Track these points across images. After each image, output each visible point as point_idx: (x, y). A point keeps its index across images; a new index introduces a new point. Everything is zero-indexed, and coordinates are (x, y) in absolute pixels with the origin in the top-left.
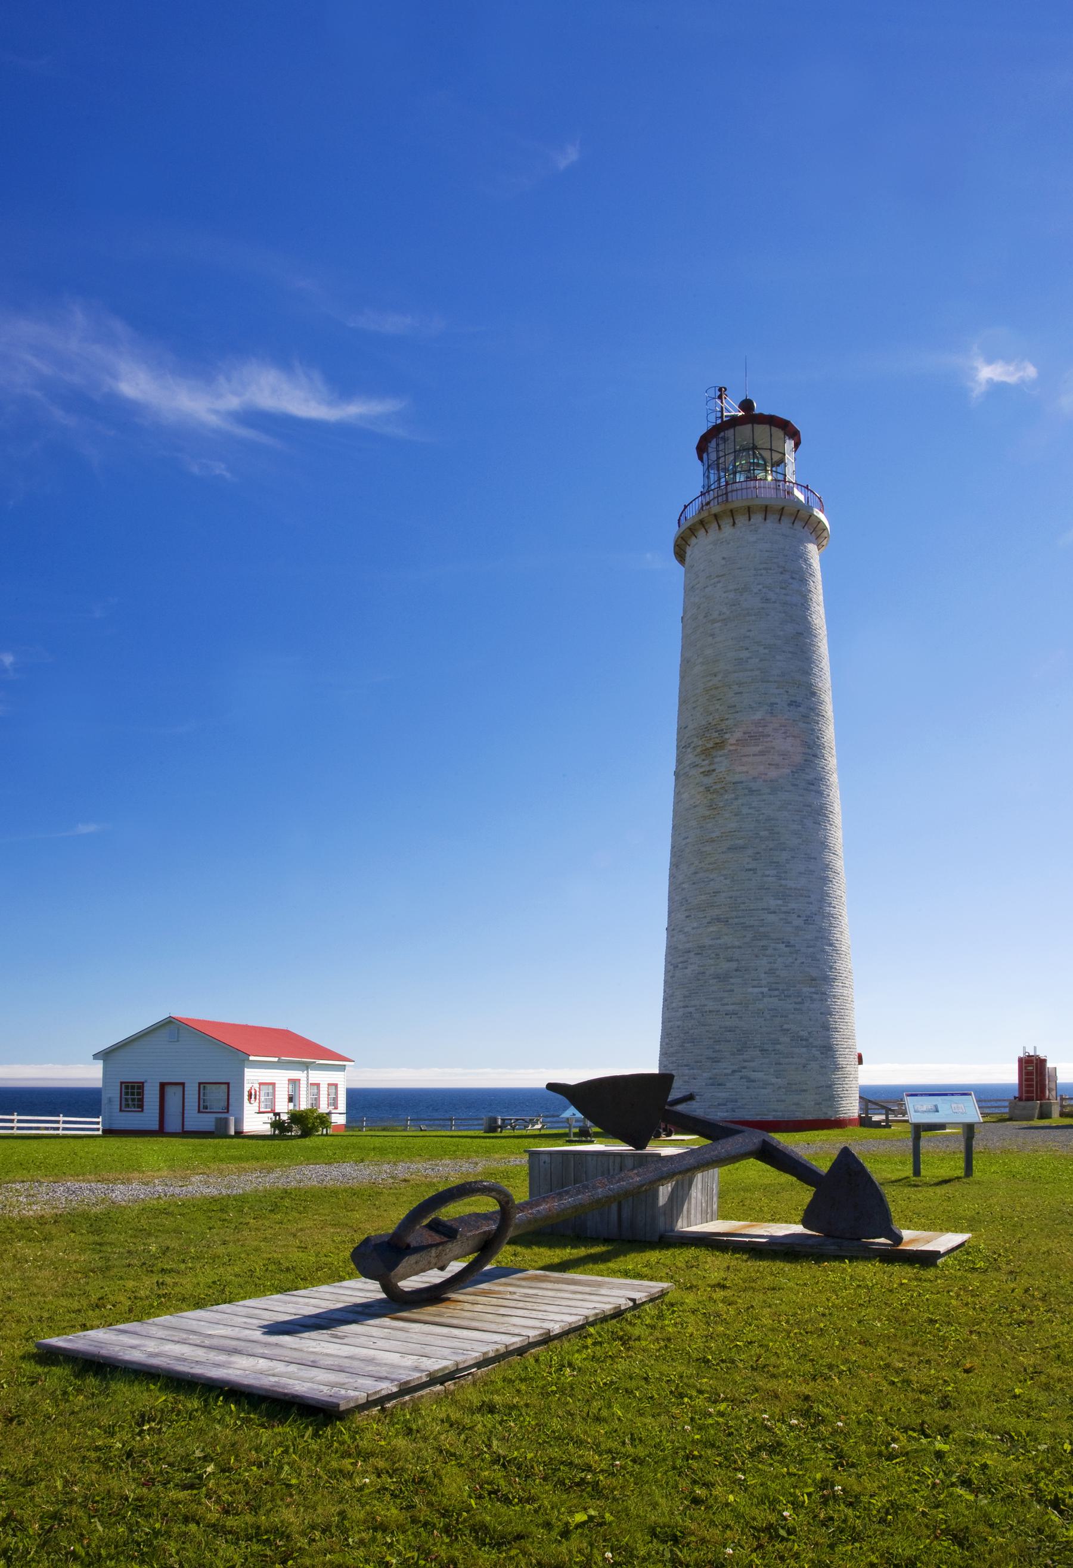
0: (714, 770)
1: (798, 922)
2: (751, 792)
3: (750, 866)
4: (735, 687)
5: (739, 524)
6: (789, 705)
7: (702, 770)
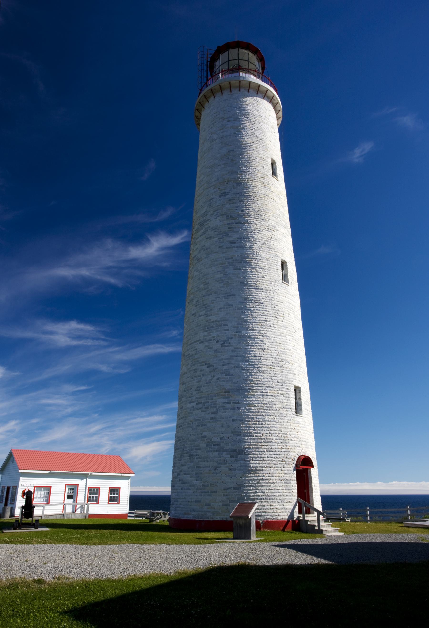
1: (217, 346)
6: (220, 196)
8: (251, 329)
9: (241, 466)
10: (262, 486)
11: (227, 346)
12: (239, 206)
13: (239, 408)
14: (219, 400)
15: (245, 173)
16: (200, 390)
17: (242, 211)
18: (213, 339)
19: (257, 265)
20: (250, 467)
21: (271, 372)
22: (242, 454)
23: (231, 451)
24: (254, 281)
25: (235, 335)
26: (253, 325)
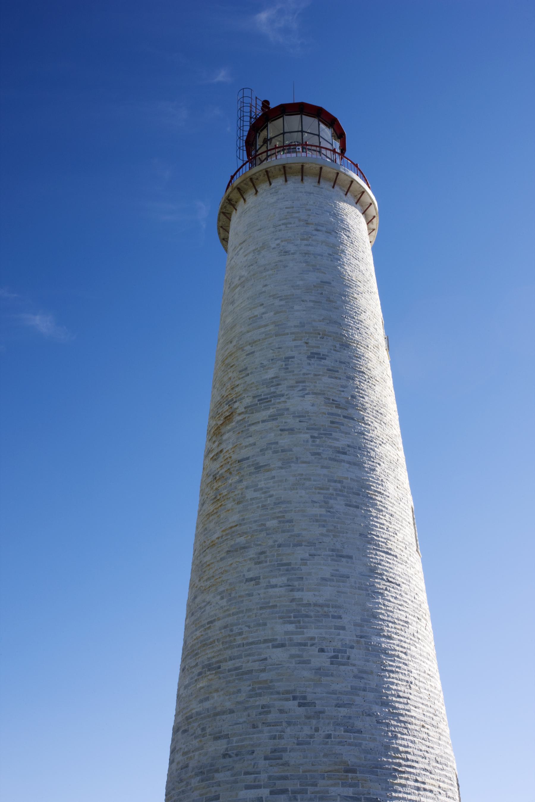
1: (321, 661)
2: (258, 468)
3: (251, 575)
4: (248, 348)
6: (309, 357)
8: (386, 634)
11: (344, 665)
14: (332, 789)
16: (280, 758)
17: (353, 397)
18: (309, 643)
19: (384, 507)
24: (382, 537)
25: (358, 642)
26: (388, 626)
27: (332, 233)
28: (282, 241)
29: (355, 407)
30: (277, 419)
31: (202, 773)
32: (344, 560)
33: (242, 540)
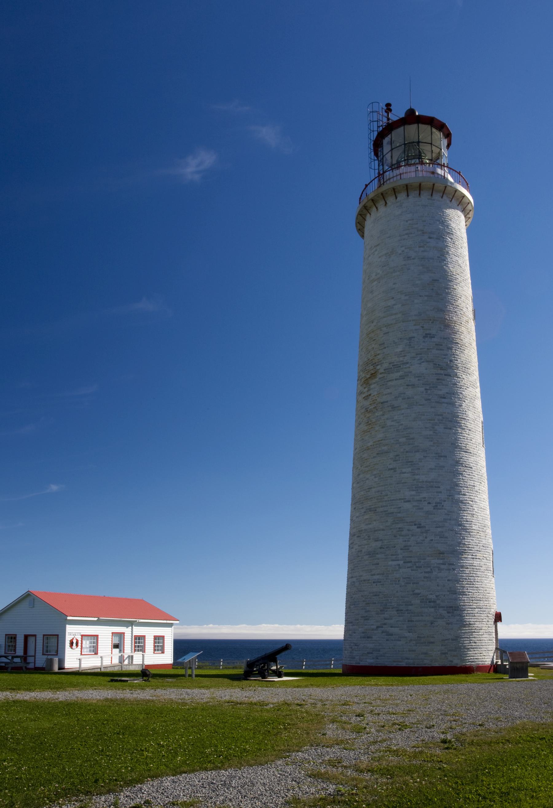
0: (370, 395)
2: (394, 408)
3: (391, 467)
4: (384, 329)
5: (389, 203)
6: (424, 337)
7: (364, 396)
9: (457, 621)
10: (475, 637)
12: (447, 355)
13: (454, 570)
15: (452, 313)
17: (451, 361)
18: (423, 500)
20: (465, 622)
21: (479, 537)
22: (458, 610)
23: (447, 607)
27: (440, 235)
28: (406, 249)
29: (451, 367)
30: (404, 378)
31: (370, 554)
32: (442, 458)
33: (385, 448)
